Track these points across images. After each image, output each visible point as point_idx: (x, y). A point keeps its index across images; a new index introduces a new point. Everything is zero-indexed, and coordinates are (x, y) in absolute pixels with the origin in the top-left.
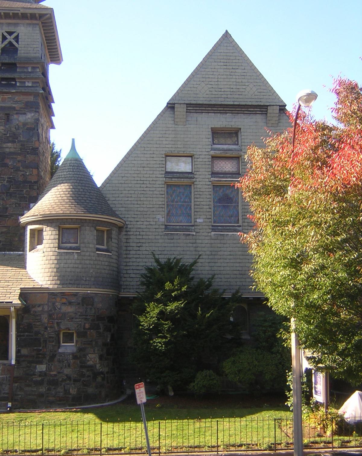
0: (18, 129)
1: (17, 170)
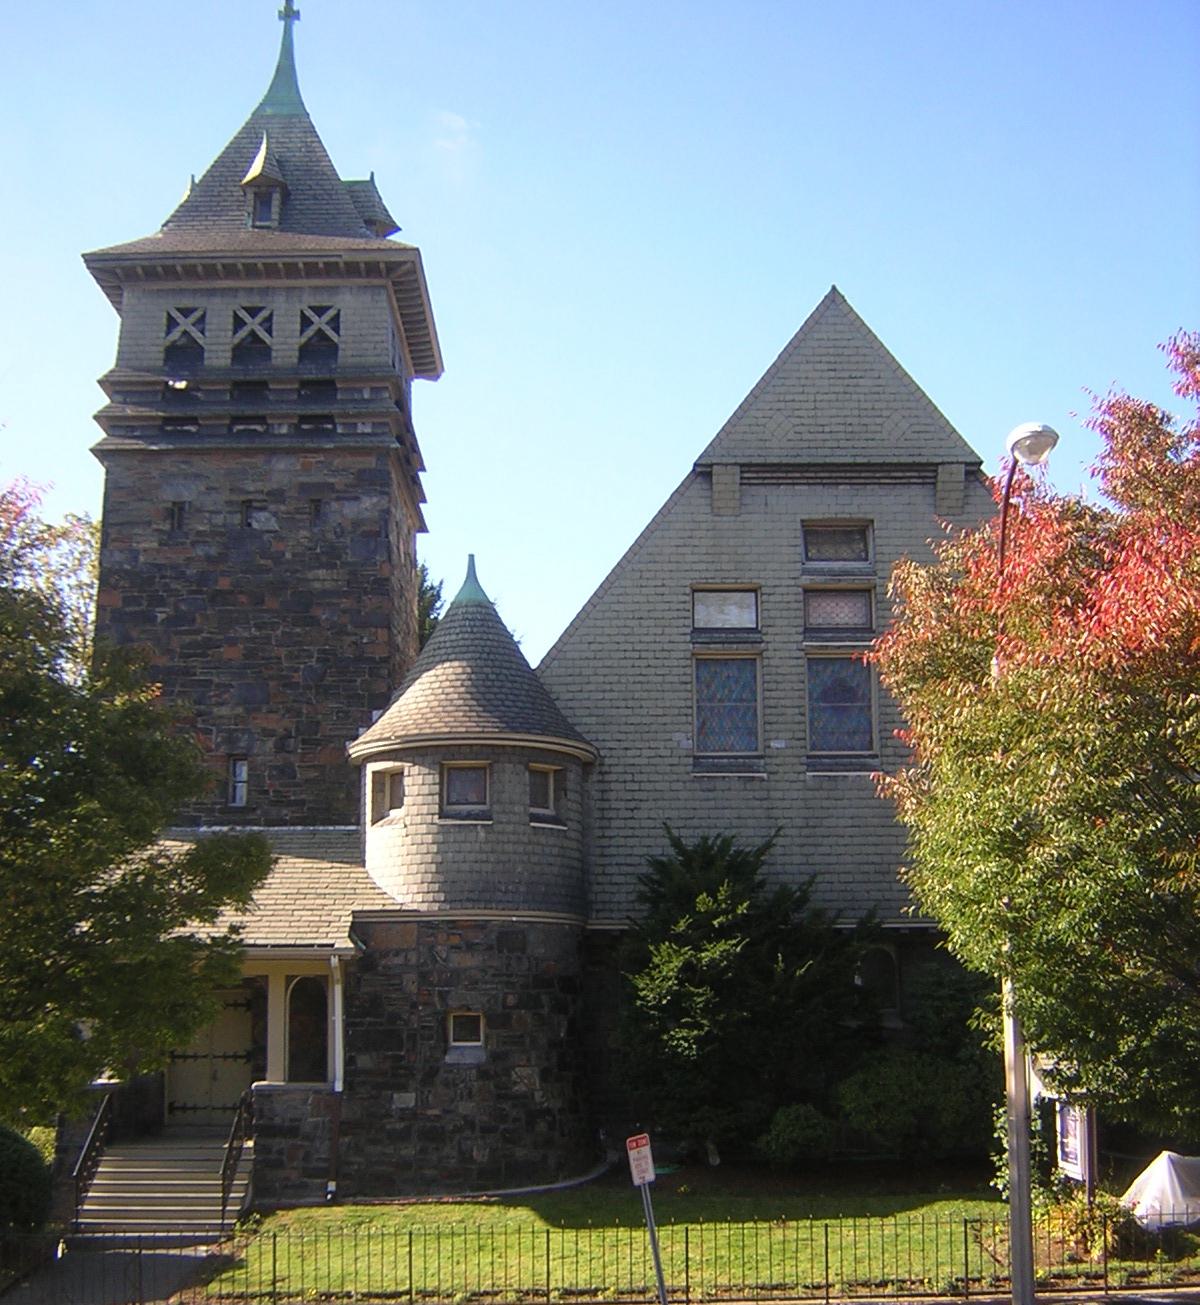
1: (341, 631)
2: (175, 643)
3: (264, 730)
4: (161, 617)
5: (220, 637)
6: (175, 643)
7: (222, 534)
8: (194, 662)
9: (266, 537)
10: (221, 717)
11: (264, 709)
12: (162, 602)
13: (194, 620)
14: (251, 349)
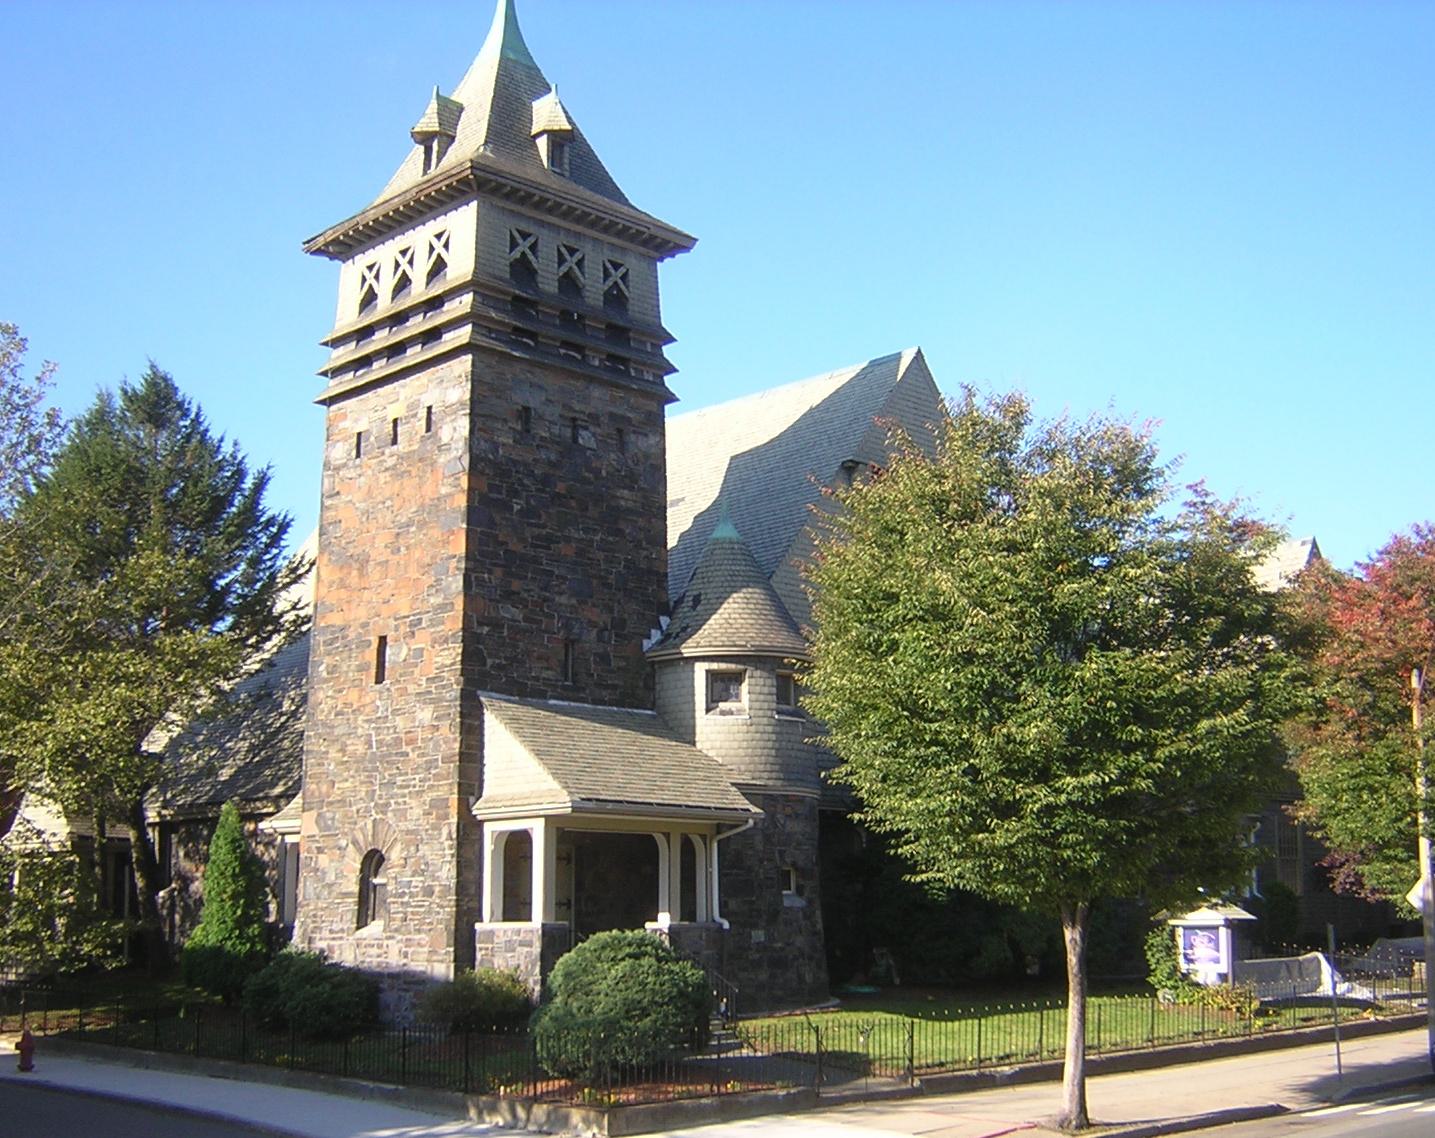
0: (636, 465)
1: (638, 546)
2: (528, 533)
3: (590, 621)
4: (516, 507)
5: (559, 534)
6: (528, 533)
7: (558, 443)
8: (542, 553)
9: (589, 453)
10: (561, 605)
11: (590, 601)
12: (516, 494)
13: (540, 517)
14: (569, 283)
